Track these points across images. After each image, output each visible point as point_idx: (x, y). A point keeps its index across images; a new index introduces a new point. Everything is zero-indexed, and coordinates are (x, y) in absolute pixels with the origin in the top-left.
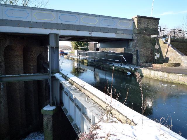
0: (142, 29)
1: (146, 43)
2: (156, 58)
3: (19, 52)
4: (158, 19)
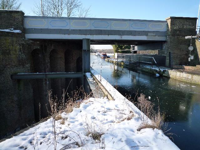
0: (176, 30)
1: (181, 44)
2: (189, 60)
3: (61, 55)
4: (195, 19)
